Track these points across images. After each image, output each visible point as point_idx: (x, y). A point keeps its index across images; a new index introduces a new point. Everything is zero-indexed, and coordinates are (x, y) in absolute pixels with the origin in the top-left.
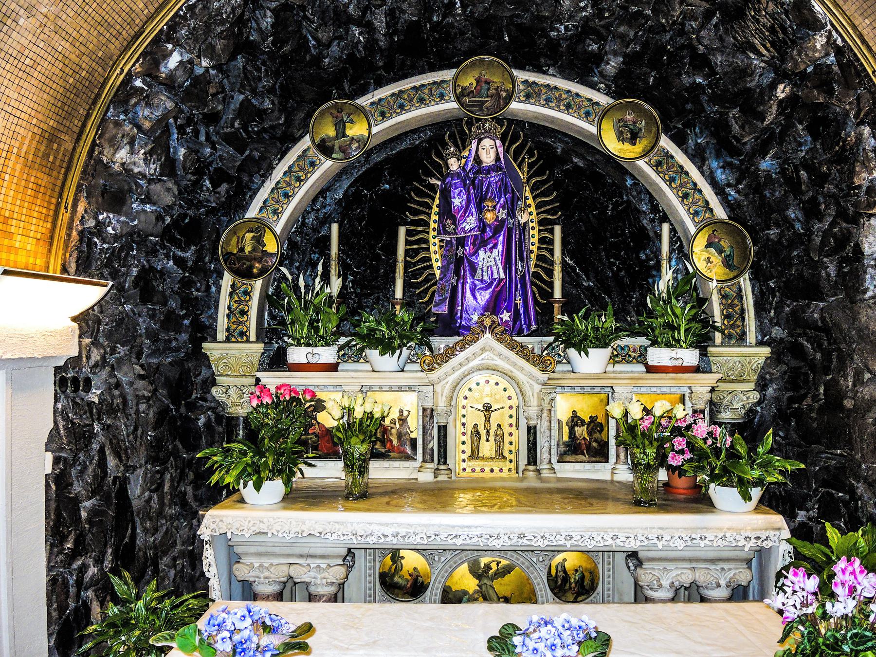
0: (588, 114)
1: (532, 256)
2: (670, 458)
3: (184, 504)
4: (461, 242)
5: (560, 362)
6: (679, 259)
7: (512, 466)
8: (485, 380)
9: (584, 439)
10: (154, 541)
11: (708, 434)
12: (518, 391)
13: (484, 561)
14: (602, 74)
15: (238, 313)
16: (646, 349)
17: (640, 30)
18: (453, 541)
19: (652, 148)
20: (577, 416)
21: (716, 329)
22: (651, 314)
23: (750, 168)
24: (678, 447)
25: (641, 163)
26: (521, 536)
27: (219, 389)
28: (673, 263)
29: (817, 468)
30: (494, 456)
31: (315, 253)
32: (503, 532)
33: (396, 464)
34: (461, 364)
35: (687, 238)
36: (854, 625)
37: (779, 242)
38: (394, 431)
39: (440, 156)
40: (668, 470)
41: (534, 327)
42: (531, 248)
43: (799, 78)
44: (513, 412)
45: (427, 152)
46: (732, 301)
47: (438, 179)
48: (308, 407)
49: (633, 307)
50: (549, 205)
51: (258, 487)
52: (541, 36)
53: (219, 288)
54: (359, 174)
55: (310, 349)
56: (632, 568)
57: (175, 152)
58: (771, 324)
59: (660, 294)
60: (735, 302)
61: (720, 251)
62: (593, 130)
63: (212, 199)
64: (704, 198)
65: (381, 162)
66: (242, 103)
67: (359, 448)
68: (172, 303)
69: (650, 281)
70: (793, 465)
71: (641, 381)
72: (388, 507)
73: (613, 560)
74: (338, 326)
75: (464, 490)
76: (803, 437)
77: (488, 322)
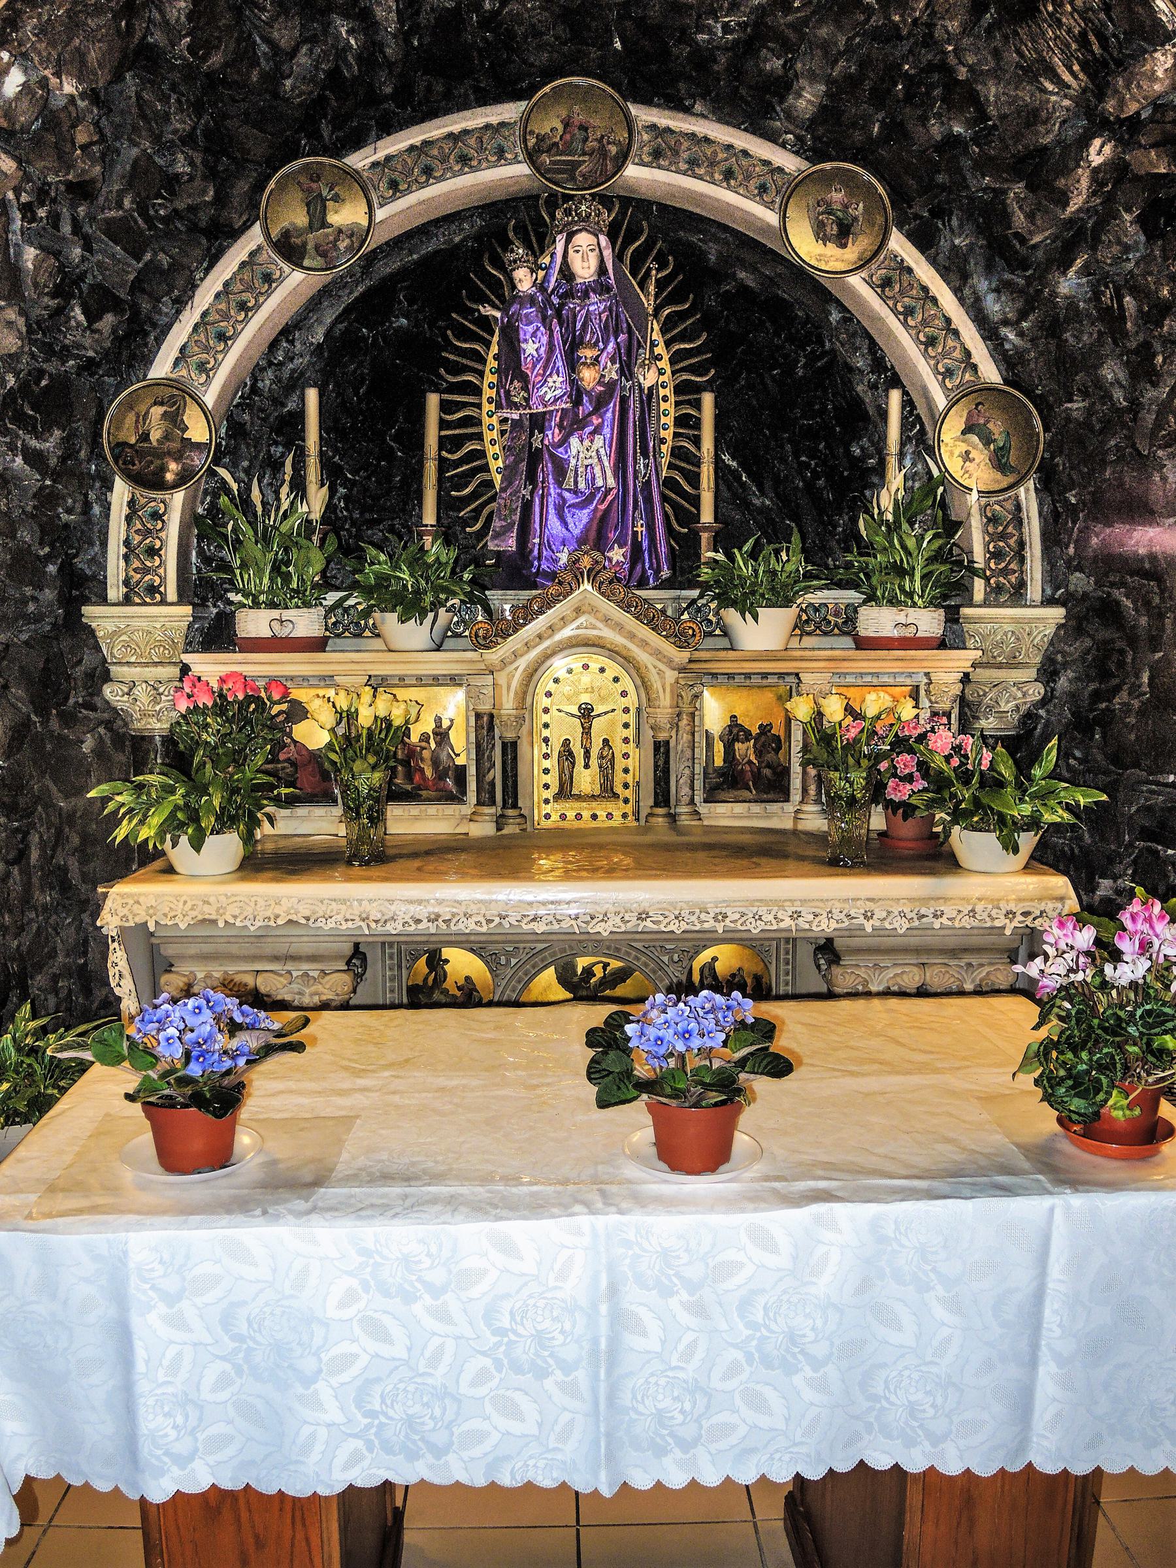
0: (763, 189)
1: (664, 448)
2: (889, 789)
3: (65, 886)
4: (538, 422)
5: (710, 634)
6: (918, 456)
7: (629, 809)
8: (580, 673)
9: (750, 762)
10: (18, 947)
11: (953, 748)
12: (639, 682)
13: (582, 963)
14: (789, 116)
15: (144, 551)
16: (856, 612)
17: (857, 34)
18: (531, 926)
19: (876, 253)
20: (738, 725)
21: (973, 572)
22: (866, 549)
23: (1041, 291)
24: (903, 771)
25: (855, 280)
26: (642, 916)
27: (116, 687)
28: (908, 462)
29: (1133, 809)
30: (597, 792)
31: (276, 443)
32: (612, 909)
33: (432, 809)
34: (540, 637)
35: (932, 416)
36: (1147, 997)
37: (1087, 425)
38: (426, 754)
39: (501, 267)
40: (886, 808)
41: (666, 573)
42: (663, 434)
43: (1126, 131)
44: (631, 718)
45: (477, 255)
46: (1003, 524)
47: (498, 309)
48: (278, 715)
49: (838, 542)
50: (696, 356)
51: (197, 844)
52: (680, 41)
53: (107, 507)
54: (353, 297)
55: (275, 613)
56: (824, 967)
57: (19, 254)
58: (1068, 568)
59: (881, 513)
60: (1010, 529)
61: (987, 440)
62: (772, 218)
63: (87, 342)
64: (962, 344)
65: (392, 275)
66: (136, 162)
67: (368, 778)
68: (25, 535)
69: (868, 493)
70: (1088, 796)
71: (846, 664)
72: (420, 875)
73: (794, 957)
74: (323, 573)
75: (549, 849)
76: (1116, 760)
77: (586, 562)
